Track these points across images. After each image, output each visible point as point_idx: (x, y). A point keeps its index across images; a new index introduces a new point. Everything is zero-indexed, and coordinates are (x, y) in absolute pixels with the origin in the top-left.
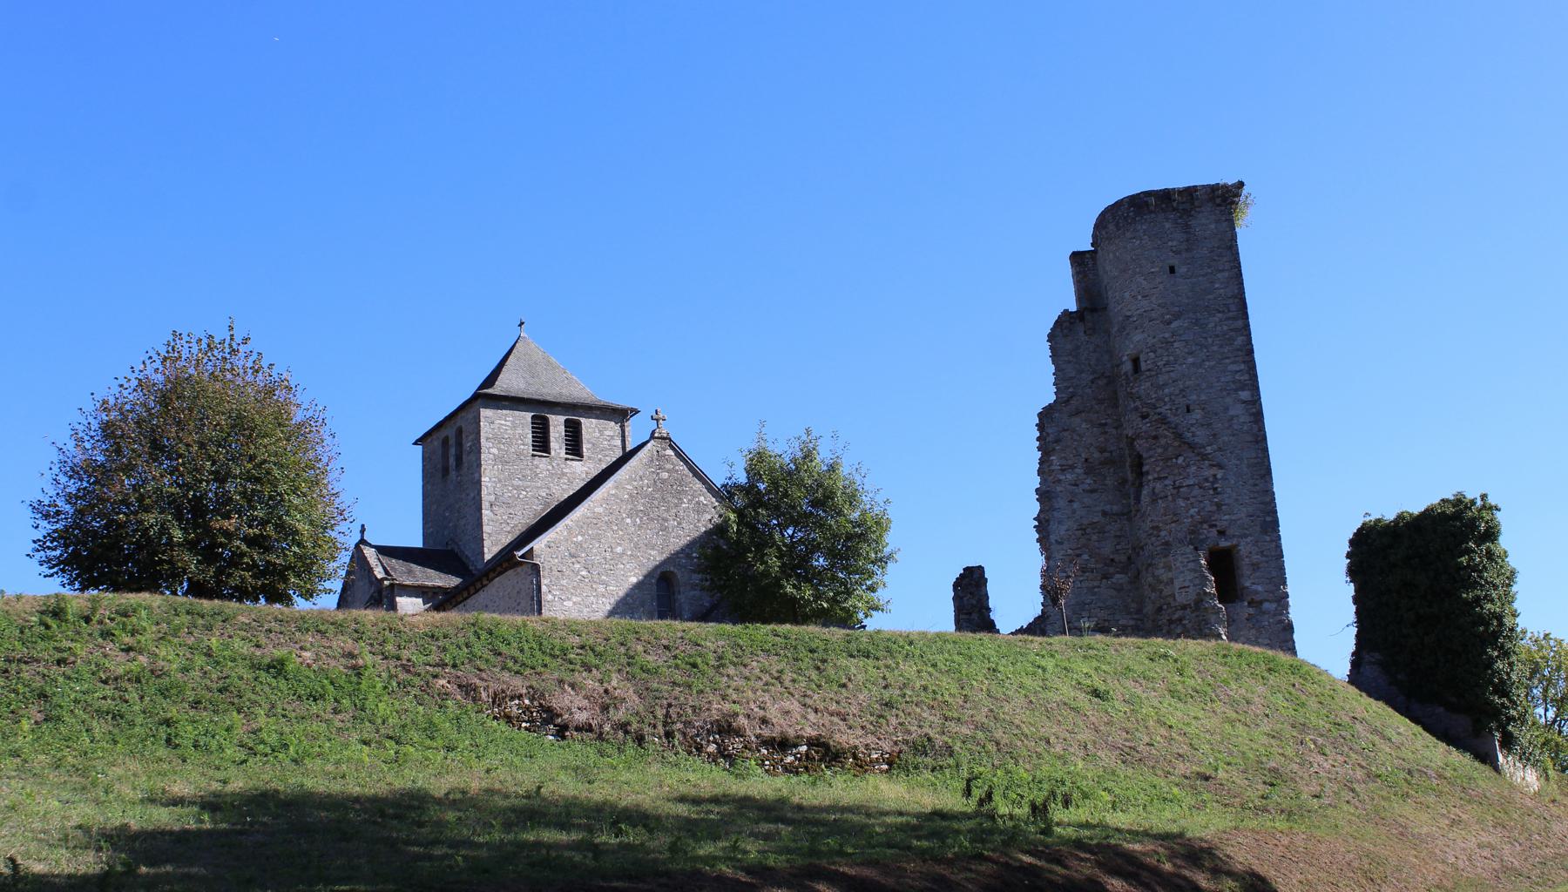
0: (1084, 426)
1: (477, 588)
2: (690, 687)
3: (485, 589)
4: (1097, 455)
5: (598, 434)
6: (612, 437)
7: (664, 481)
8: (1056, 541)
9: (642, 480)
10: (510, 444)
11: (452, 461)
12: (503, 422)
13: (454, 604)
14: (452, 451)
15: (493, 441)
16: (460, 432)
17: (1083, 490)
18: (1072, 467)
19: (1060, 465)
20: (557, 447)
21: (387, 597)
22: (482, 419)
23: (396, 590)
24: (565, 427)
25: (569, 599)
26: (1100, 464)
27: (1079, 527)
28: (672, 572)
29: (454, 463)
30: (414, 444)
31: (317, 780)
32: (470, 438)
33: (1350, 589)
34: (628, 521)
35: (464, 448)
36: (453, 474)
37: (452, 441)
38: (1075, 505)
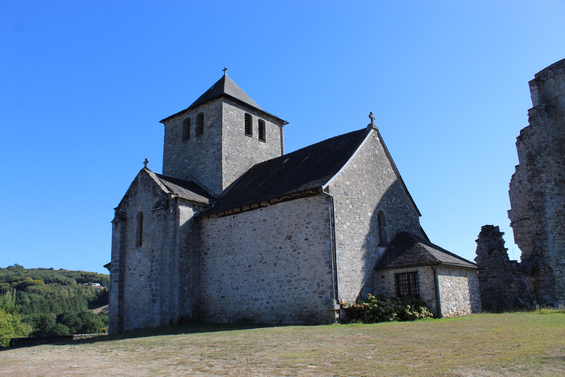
0: (552, 161)
1: (244, 210)
2: (274, 253)
4: (558, 177)
5: (271, 130)
8: (549, 218)
10: (235, 126)
12: (232, 113)
13: (219, 215)
15: (228, 122)
16: (201, 117)
17: (555, 193)
18: (550, 181)
19: (546, 180)
20: (255, 133)
21: (172, 205)
22: (223, 109)
23: (178, 201)
26: (560, 182)
27: (556, 212)
29: (195, 133)
30: (160, 122)
31: (122, 340)
33: (125, 195)
36: (193, 139)
38: (554, 200)
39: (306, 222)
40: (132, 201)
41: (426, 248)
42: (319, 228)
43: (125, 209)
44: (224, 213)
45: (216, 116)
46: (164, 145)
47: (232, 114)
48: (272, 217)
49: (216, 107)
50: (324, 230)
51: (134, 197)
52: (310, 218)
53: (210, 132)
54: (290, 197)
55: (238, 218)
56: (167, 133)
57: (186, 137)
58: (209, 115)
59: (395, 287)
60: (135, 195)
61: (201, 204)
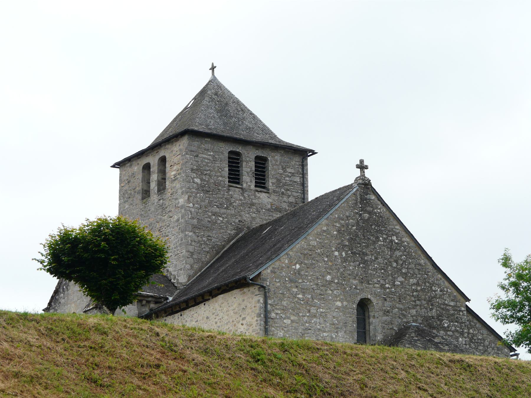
1: (190, 305)
3: (207, 303)
5: (281, 171)
6: (293, 174)
7: (365, 221)
9: (348, 220)
11: (153, 186)
14: (154, 177)
16: (163, 160)
24: (256, 163)
25: (289, 318)
28: (369, 299)
29: (156, 188)
30: (112, 167)
32: (175, 167)
33: (55, 289)
34: (336, 253)
35: (168, 175)
36: (154, 197)
37: (154, 168)
39: (241, 318)
40: (64, 298)
41: (190, 324)
42: (252, 325)
43: (56, 310)
44: (172, 310)
45: (180, 164)
46: (120, 205)
47: (205, 158)
48: (213, 314)
49: (180, 150)
50: (256, 326)
51: (66, 292)
52: (245, 313)
53: (174, 187)
54: (227, 288)
55: (185, 316)
56: (123, 185)
57: (146, 193)
58: (172, 160)
59: (29, 312)
60: (68, 290)
61: (150, 299)
